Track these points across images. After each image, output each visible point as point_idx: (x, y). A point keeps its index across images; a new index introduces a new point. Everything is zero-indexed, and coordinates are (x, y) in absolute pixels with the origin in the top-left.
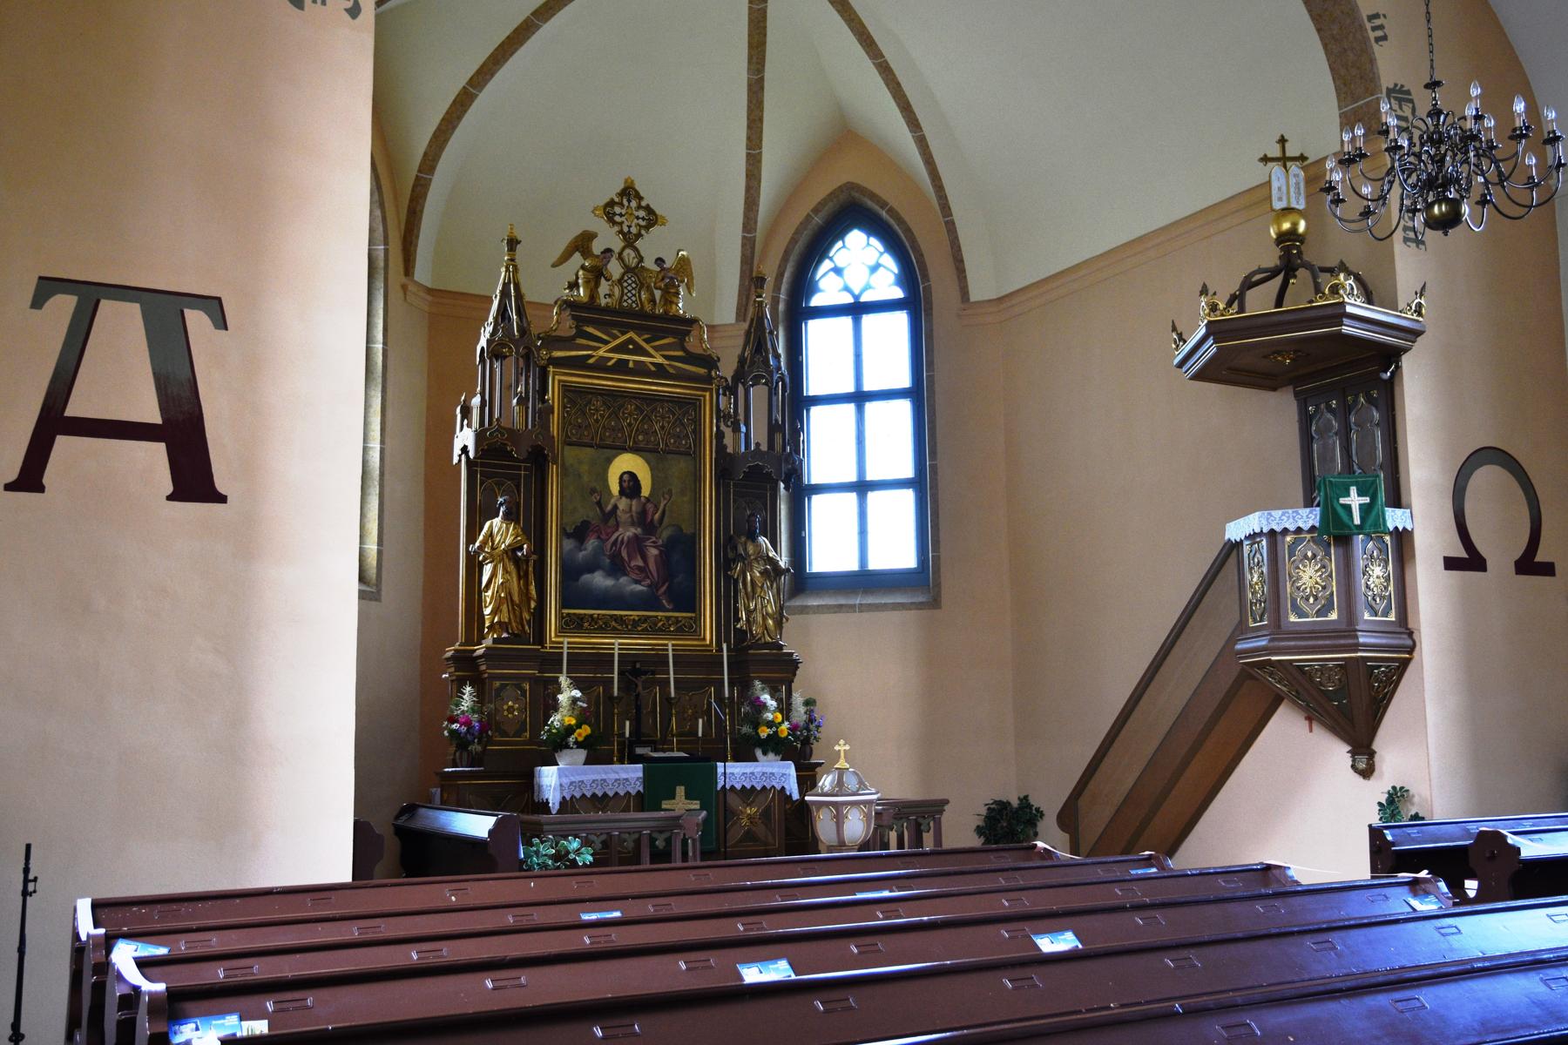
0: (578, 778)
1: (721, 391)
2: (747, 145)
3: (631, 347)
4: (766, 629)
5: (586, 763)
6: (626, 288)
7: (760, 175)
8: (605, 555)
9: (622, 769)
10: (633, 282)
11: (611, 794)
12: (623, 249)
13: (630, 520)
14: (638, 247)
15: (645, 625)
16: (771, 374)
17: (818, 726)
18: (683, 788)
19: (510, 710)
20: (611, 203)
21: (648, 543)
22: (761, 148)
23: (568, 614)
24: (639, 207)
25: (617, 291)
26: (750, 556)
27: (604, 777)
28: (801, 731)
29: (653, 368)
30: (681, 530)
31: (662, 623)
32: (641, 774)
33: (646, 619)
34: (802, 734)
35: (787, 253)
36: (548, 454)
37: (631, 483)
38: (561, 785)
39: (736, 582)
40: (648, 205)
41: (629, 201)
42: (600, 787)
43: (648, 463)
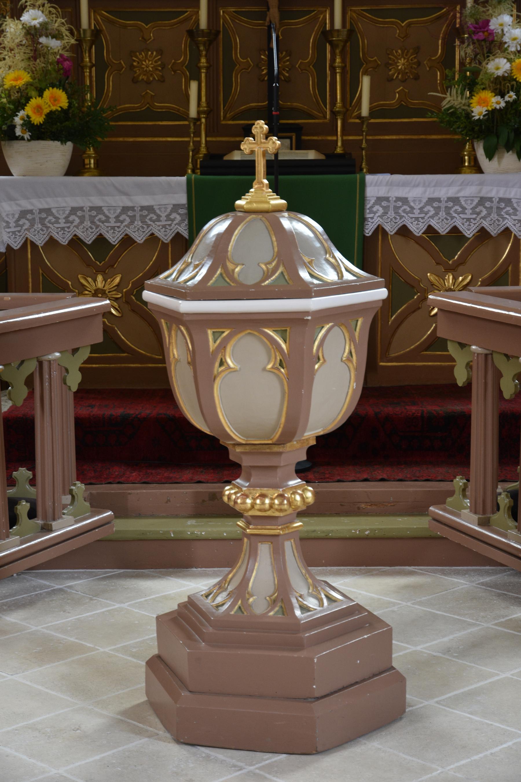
0: (38, 204)
11: (114, 238)
27: (97, 201)
32: (182, 199)
42: (87, 223)
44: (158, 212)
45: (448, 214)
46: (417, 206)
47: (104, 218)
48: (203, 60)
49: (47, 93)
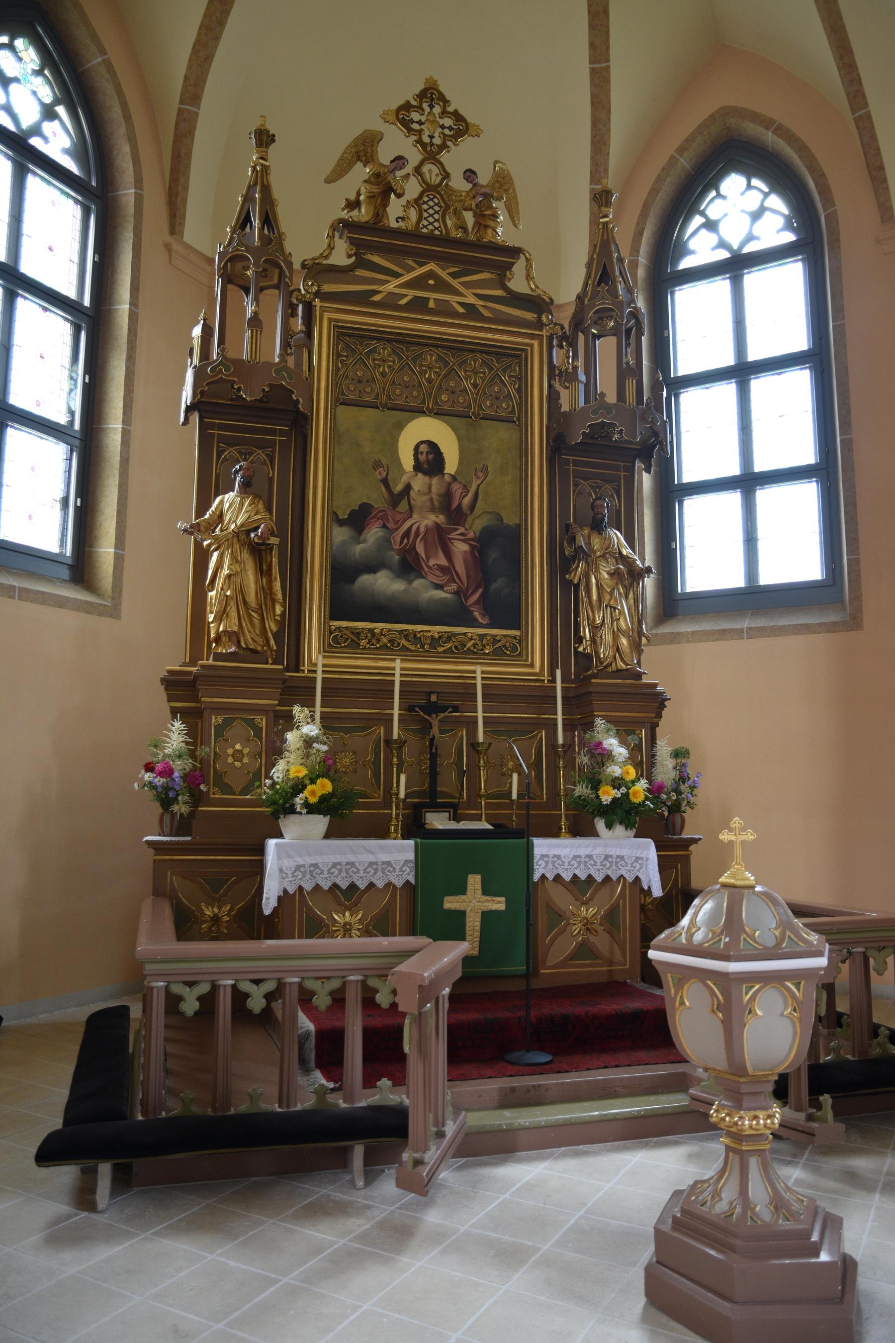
0: (309, 860)
1: (555, 343)
2: (590, 56)
3: (431, 282)
4: (618, 650)
5: (327, 836)
6: (426, 211)
7: (609, 102)
8: (393, 549)
9: (381, 847)
10: (436, 204)
11: (362, 885)
12: (422, 163)
13: (428, 504)
14: (442, 160)
15: (448, 646)
16: (620, 305)
17: (693, 788)
18: (478, 878)
19: (238, 756)
20: (407, 107)
21: (454, 535)
22: (608, 61)
23: (338, 628)
24: (444, 113)
25: (413, 214)
26: (594, 552)
27: (351, 858)
28: (668, 794)
29: (461, 310)
30: (501, 519)
31: (472, 642)
32: (411, 856)
33: (450, 637)
34: (669, 798)
35: (646, 207)
36: (298, 400)
37: (431, 456)
38: (281, 870)
39: (577, 587)
40: (456, 111)
41: (431, 107)
42: (344, 874)
43: (455, 429)
44: (394, 865)
45: (586, 866)
46: (567, 861)
47: (356, 870)
48: (395, 759)
49: (319, 781)
